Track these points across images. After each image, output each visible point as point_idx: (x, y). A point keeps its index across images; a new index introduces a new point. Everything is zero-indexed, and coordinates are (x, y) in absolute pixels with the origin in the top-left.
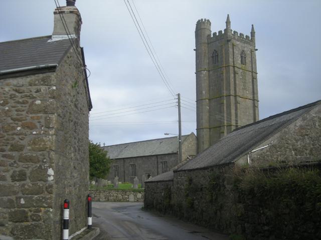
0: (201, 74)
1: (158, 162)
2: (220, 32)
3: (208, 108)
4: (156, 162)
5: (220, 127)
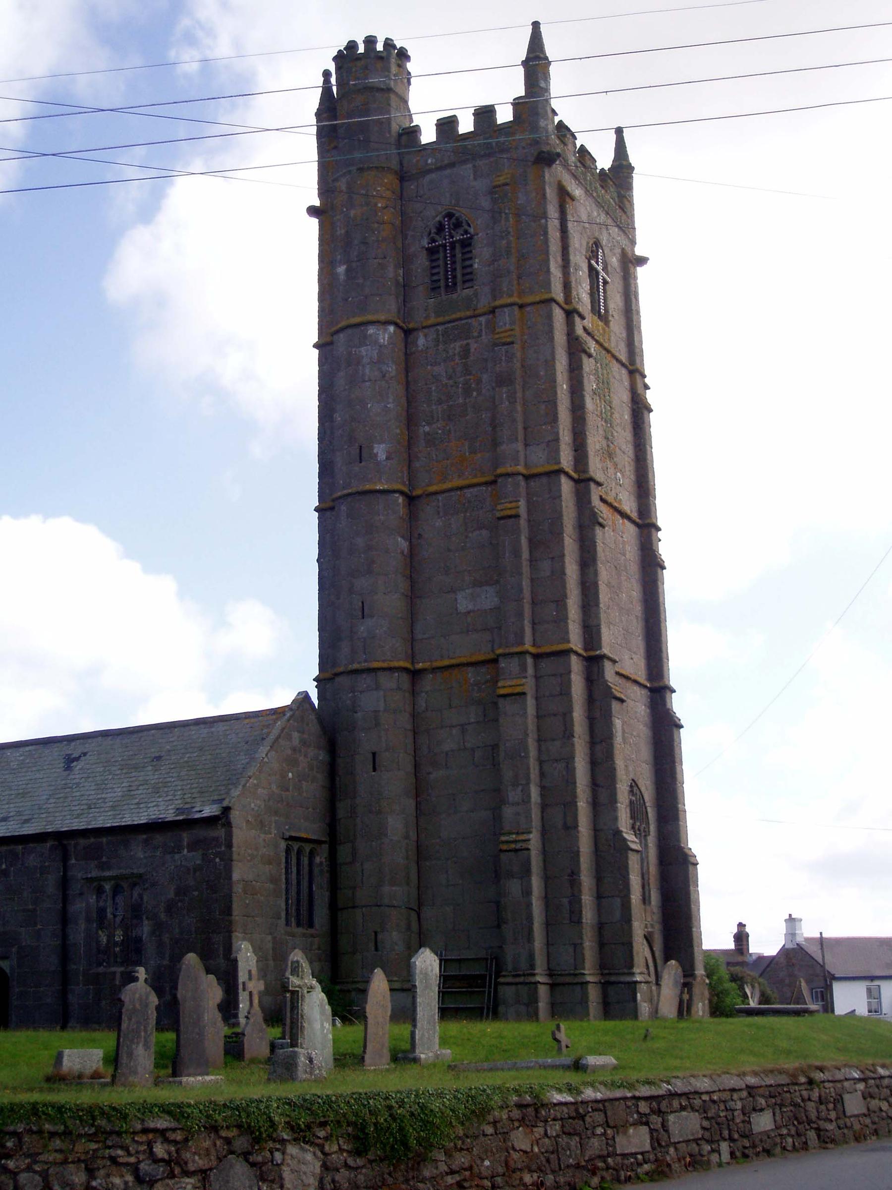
0: (364, 340)
1: (65, 883)
2: (485, 114)
3: (403, 544)
4: (51, 883)
5: (495, 661)
